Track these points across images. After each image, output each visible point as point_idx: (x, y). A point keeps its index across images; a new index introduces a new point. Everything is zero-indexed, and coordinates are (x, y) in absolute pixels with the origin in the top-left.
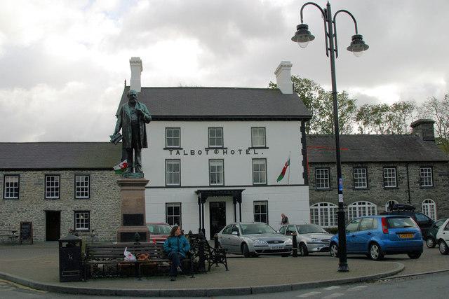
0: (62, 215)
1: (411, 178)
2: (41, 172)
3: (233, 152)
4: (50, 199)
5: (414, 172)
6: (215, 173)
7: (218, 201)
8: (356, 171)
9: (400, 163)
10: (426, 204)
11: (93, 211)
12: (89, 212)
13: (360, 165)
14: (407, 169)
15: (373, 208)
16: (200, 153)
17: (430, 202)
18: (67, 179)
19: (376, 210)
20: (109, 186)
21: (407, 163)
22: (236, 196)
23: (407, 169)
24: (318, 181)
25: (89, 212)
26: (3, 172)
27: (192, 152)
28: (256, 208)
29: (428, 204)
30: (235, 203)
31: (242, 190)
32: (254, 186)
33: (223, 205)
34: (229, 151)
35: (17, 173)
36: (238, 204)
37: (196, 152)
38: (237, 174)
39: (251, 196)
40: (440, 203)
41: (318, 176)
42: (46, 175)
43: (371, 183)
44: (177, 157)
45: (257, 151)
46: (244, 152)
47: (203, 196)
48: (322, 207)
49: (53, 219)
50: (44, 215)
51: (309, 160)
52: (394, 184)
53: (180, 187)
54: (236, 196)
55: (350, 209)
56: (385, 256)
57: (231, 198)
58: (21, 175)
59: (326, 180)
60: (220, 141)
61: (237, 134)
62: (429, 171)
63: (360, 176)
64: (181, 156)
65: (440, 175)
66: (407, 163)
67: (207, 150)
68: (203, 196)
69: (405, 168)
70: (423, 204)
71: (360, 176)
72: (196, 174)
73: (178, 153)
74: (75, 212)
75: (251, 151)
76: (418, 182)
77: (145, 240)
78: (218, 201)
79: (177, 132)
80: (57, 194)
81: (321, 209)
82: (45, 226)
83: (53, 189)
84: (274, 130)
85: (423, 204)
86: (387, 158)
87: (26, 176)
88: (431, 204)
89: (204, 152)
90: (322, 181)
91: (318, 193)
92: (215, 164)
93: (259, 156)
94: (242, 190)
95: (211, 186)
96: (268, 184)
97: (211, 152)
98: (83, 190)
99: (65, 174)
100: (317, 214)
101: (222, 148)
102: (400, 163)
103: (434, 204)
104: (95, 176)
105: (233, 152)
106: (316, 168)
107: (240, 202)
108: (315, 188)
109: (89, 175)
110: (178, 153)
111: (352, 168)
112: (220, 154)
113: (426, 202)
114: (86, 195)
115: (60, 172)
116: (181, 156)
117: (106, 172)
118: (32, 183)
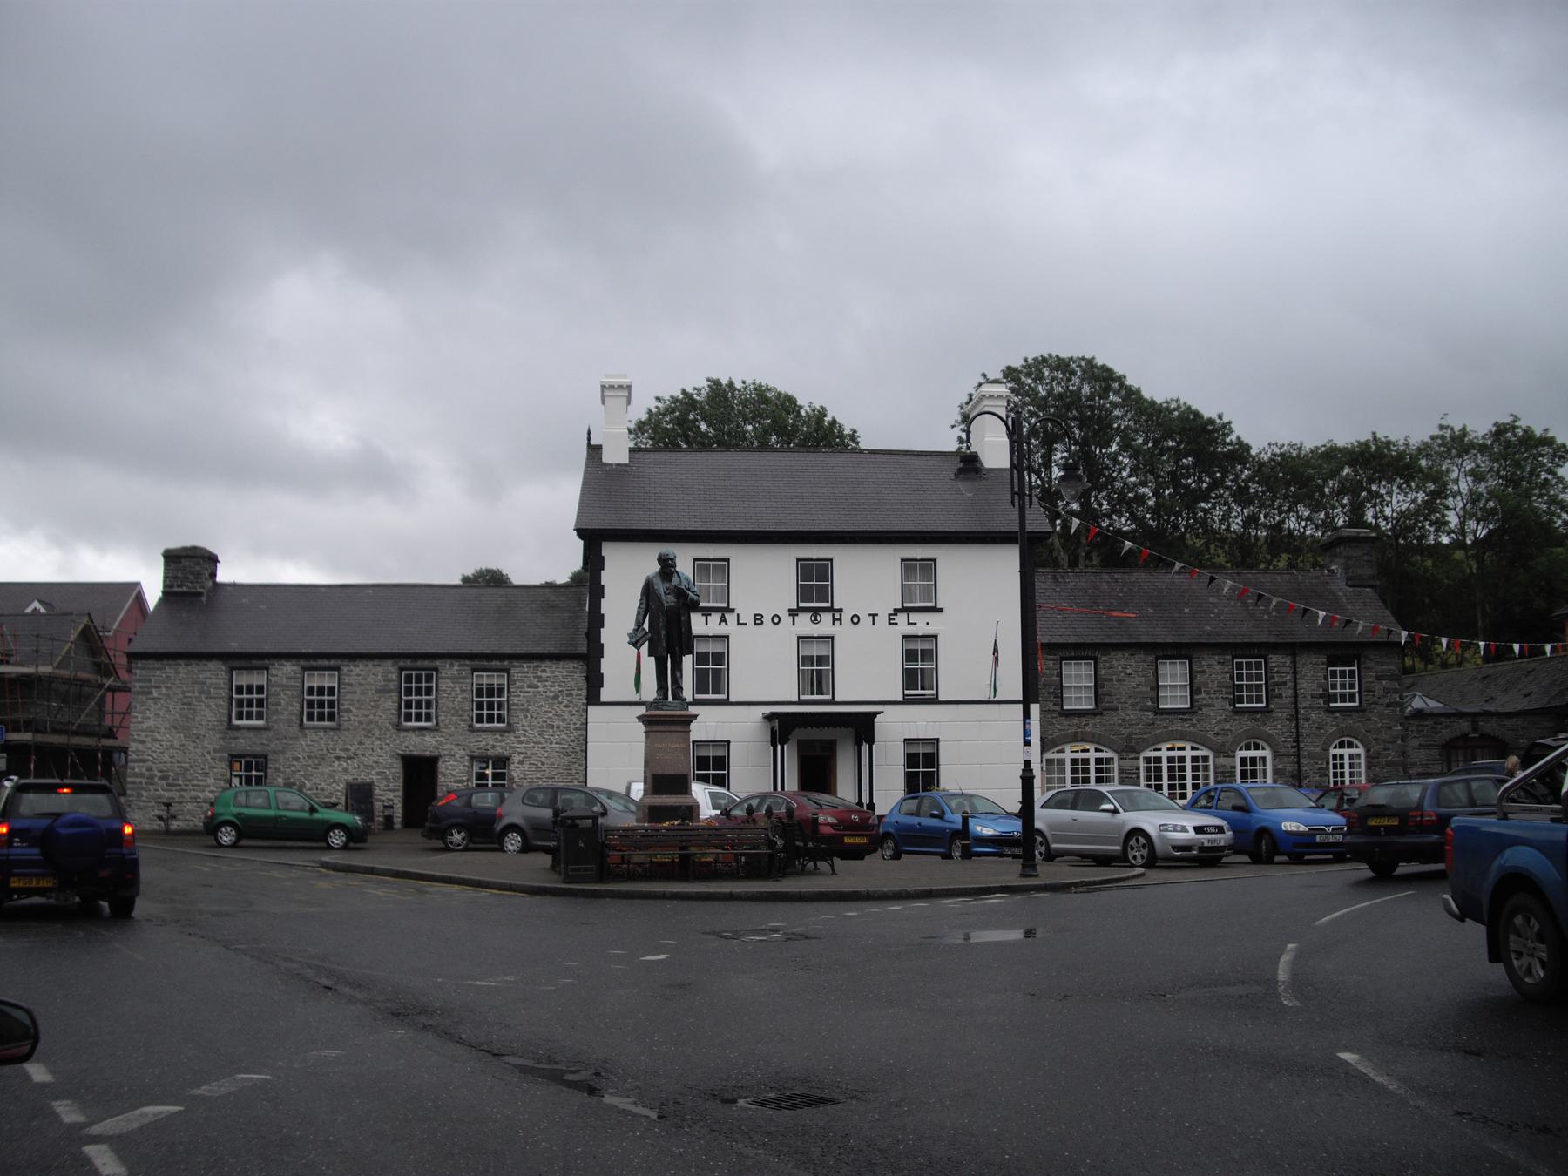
0: (441, 766)
1: (1304, 685)
2: (390, 663)
3: (758, 620)
4: (414, 729)
5: (1311, 671)
6: (816, 669)
7: (818, 737)
8: (1240, 666)
9: (1275, 647)
10: (1338, 751)
11: (516, 758)
12: (508, 759)
13: (1173, 652)
14: (1294, 663)
15: (1205, 759)
16: (776, 619)
17: (1350, 745)
18: (454, 679)
19: (1269, 768)
20: (556, 697)
21: (1293, 649)
22: (861, 727)
23: (1294, 663)
24: (1240, 688)
25: (508, 759)
26: (302, 662)
27: (758, 620)
28: (911, 760)
29: (1346, 752)
30: (859, 745)
31: (875, 714)
32: (907, 701)
33: (830, 748)
34: (846, 617)
35: (333, 663)
36: (865, 748)
37: (767, 620)
38: (866, 672)
39: (898, 726)
40: (1376, 748)
41: (1240, 677)
42: (401, 669)
43: (1202, 697)
44: (722, 630)
45: (914, 617)
46: (882, 620)
47: (782, 727)
48: (1172, 753)
49: (419, 773)
50: (398, 767)
51: (1042, 638)
52: (1259, 700)
53: (726, 702)
54: (861, 727)
55: (1148, 760)
56: (1403, 869)
57: (850, 731)
58: (345, 670)
59: (1259, 688)
60: (825, 593)
61: (866, 578)
62: (1258, 666)
63: (1249, 677)
64: (730, 628)
65: (1379, 678)
66: (1293, 649)
67: (793, 613)
68: (782, 727)
69: (1288, 661)
70: (1333, 751)
71: (1249, 677)
72: (763, 668)
73: (723, 620)
74: (472, 758)
75: (901, 618)
76: (1321, 696)
77: (691, 820)
78: (818, 737)
79: (929, 566)
80: (331, 717)
81: (1170, 760)
82: (400, 793)
83: (415, 701)
84: (954, 564)
85: (1333, 751)
86: (1246, 631)
87: (355, 671)
88: (1354, 751)
89: (786, 619)
90: (1249, 688)
91: (1065, 721)
92: (816, 650)
93: (920, 629)
94: (875, 714)
95: (801, 702)
96: (941, 698)
97: (804, 618)
98: (489, 708)
99: (450, 670)
100: (1183, 769)
101: (831, 610)
102: (1275, 647)
103: (1361, 751)
104: (523, 674)
105: (855, 621)
106: (1063, 659)
107: (871, 742)
108: (1058, 708)
109: (436, 670)
110: (723, 620)
111: (1151, 658)
112: (825, 626)
113: (1341, 745)
114: (428, 719)
115: (438, 663)
116: (730, 628)
117: (548, 663)
118: (367, 691)
